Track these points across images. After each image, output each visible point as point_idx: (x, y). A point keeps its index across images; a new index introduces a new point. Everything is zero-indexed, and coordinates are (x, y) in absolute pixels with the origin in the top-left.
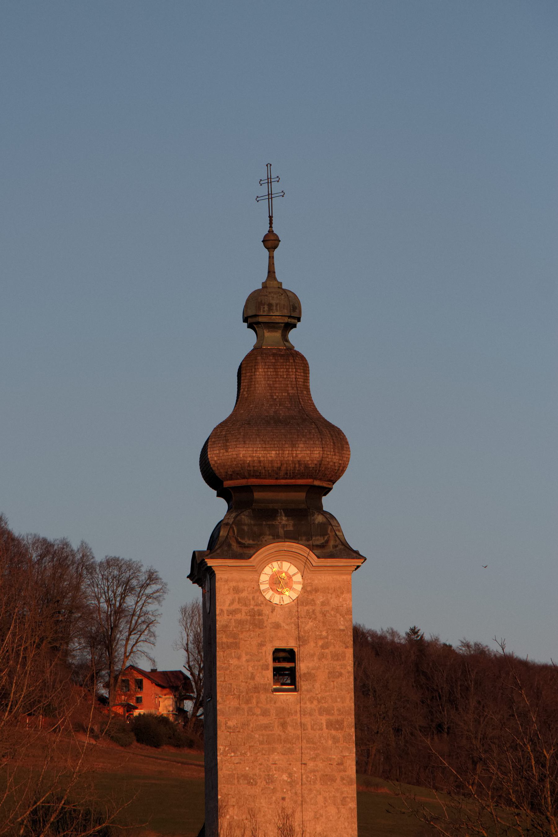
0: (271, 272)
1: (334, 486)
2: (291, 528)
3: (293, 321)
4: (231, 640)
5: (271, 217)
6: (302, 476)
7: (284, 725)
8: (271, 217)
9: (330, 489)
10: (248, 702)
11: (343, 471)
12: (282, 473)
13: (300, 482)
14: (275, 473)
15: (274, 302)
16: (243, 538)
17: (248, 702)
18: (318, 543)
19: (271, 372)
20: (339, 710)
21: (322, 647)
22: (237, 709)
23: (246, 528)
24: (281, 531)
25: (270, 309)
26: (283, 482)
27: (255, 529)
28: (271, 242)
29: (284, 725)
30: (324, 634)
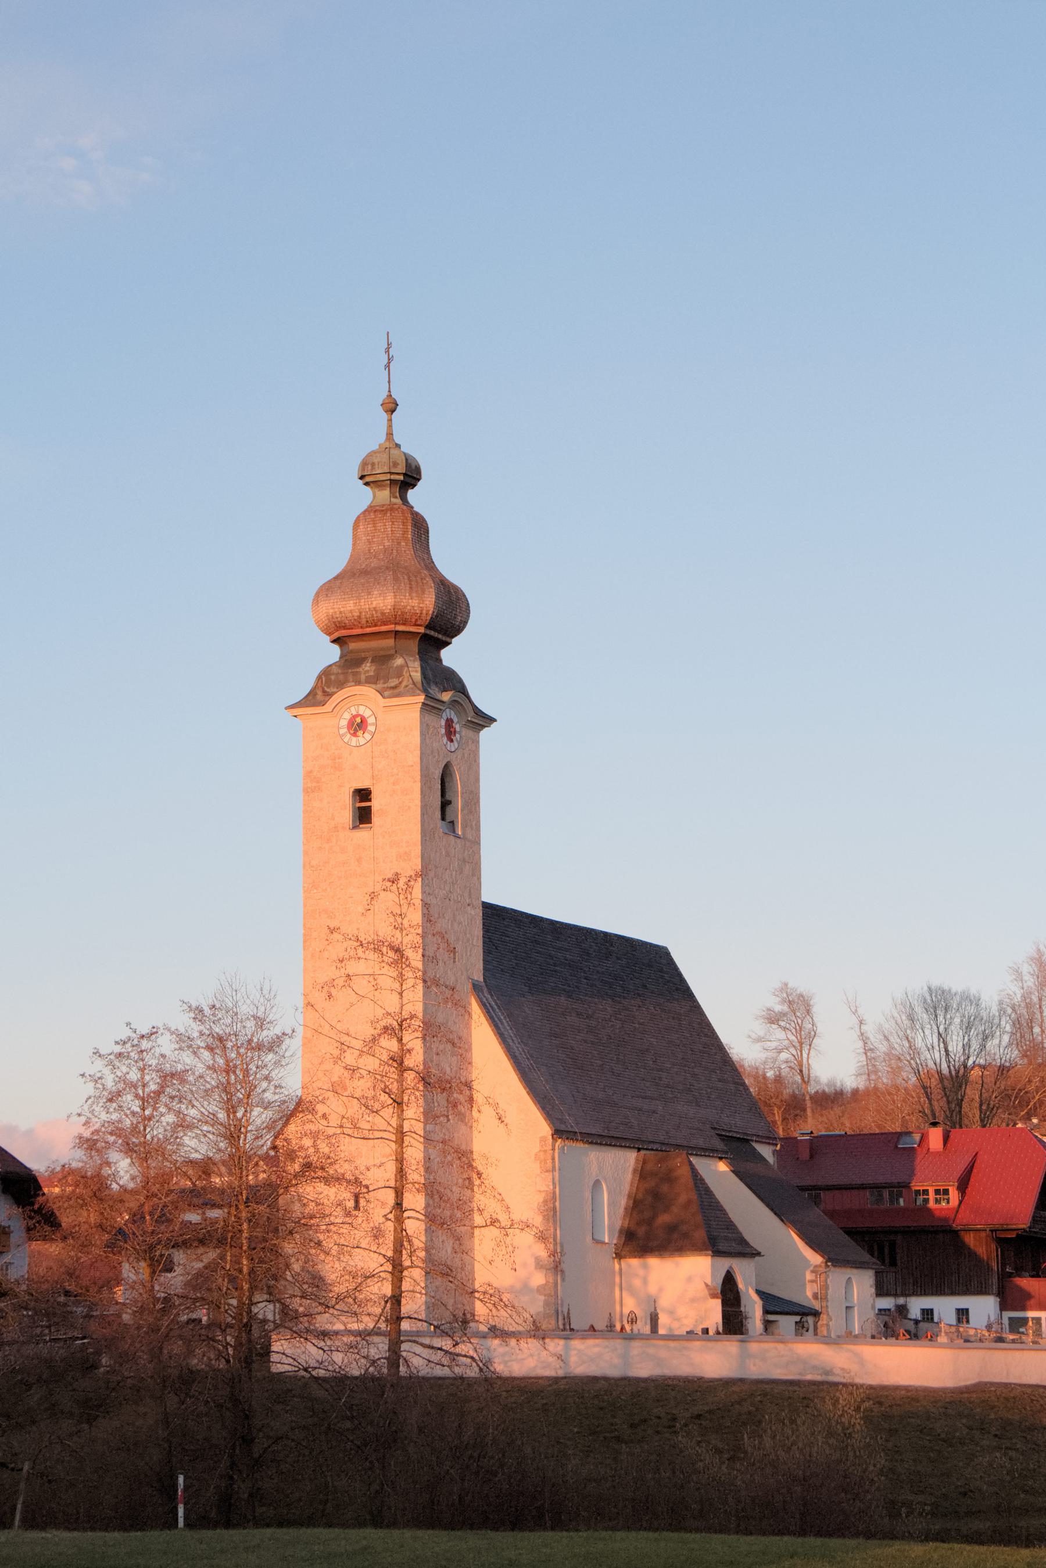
0: (390, 434)
1: (454, 640)
2: (372, 673)
3: (409, 480)
4: (314, 784)
5: (389, 382)
6: (385, 624)
7: (359, 860)
8: (389, 382)
9: (450, 643)
10: (329, 840)
11: (464, 627)
12: (364, 621)
13: (384, 628)
14: (357, 622)
15: (376, 461)
16: (328, 687)
17: (329, 840)
18: (393, 685)
19: (370, 528)
20: (407, 842)
21: (394, 784)
22: (320, 848)
23: (333, 677)
24: (363, 677)
25: (373, 468)
26: (368, 630)
27: (341, 677)
28: (391, 407)
29: (359, 860)
30: (395, 771)
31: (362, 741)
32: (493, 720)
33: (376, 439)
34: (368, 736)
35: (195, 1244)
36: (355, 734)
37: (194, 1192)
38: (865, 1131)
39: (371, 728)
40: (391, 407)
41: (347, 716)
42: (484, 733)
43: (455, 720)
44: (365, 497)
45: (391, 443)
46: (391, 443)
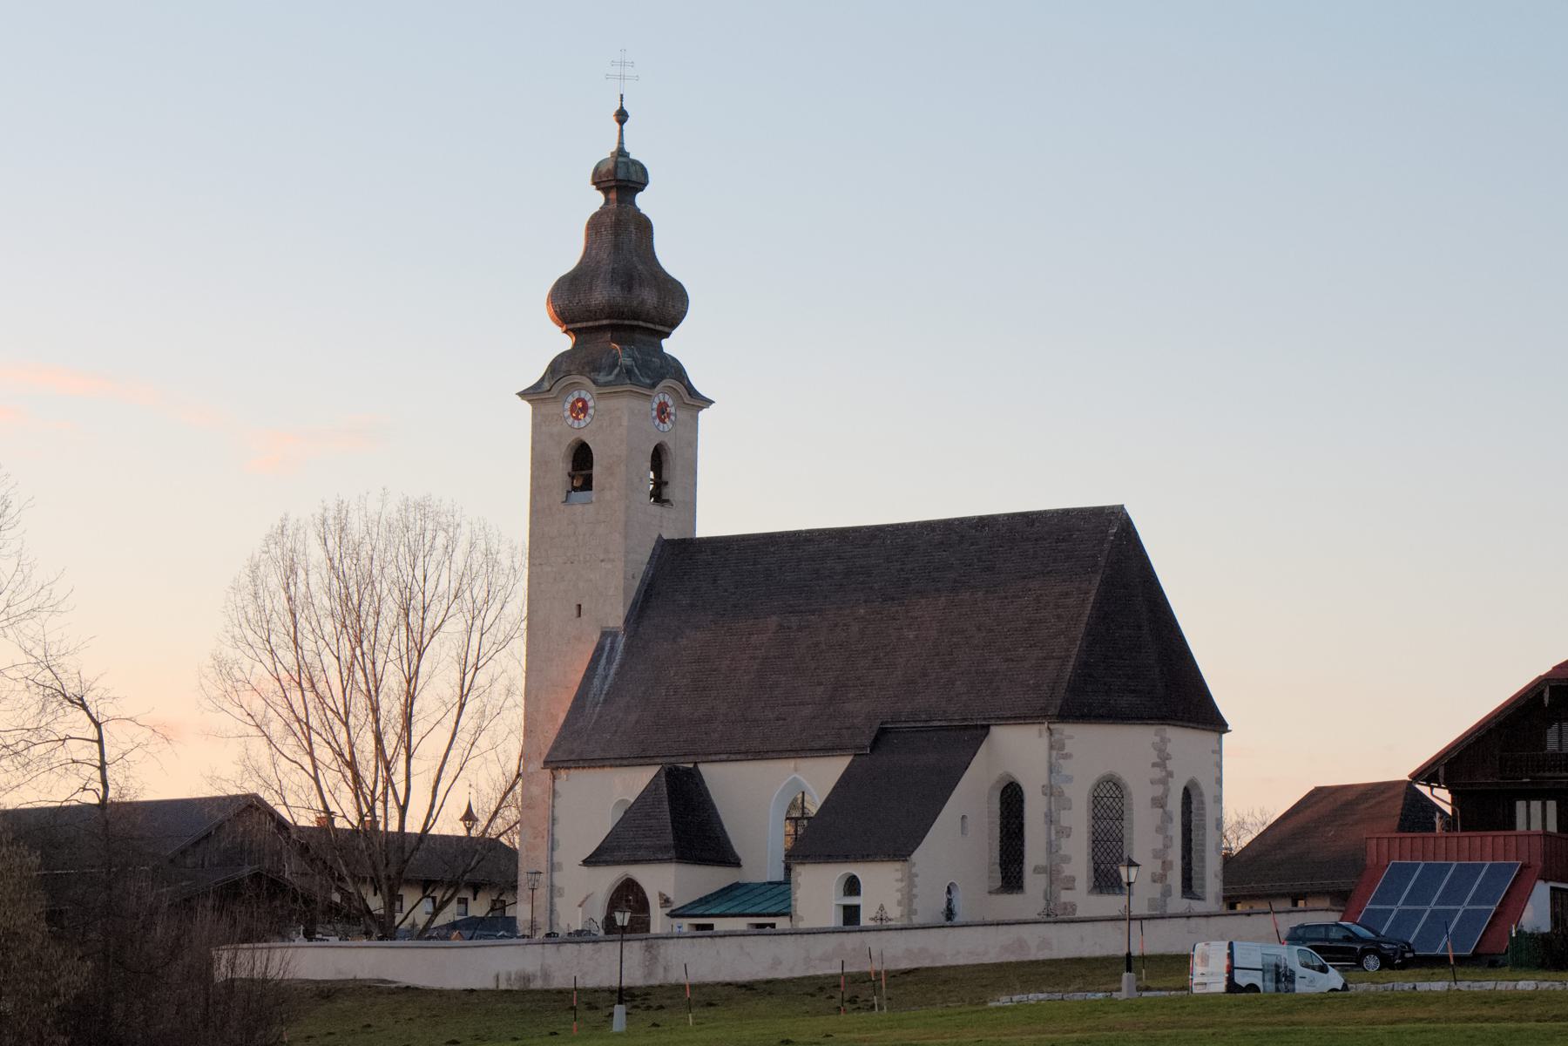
0: (621, 142)
28: (622, 116)
31: (583, 424)
32: (711, 402)
33: (606, 150)
34: (588, 419)
35: (1372, 962)
36: (577, 418)
37: (613, 311)
38: (537, 984)
39: (591, 411)
40: (622, 116)
41: (571, 399)
42: (703, 415)
43: (670, 403)
44: (597, 200)
45: (621, 152)
46: (621, 152)
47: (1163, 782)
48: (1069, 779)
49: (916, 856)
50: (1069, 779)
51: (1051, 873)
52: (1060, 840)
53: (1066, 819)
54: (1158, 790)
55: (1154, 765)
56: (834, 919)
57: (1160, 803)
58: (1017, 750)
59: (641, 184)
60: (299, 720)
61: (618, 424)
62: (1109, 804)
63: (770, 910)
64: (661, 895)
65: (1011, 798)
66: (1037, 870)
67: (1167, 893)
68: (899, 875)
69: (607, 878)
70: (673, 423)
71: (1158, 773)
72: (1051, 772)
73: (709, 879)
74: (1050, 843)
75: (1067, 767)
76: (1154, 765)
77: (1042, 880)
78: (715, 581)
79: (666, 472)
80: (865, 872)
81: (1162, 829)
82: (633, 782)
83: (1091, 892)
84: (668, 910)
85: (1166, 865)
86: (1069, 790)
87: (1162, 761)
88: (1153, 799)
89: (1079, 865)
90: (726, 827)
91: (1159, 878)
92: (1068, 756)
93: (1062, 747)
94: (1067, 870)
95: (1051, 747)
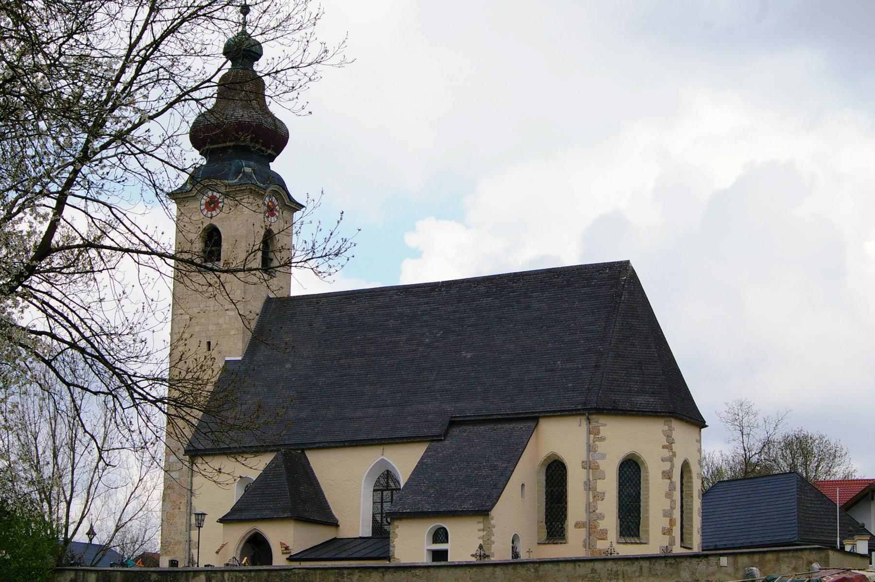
47: (670, 459)
48: (603, 456)
49: (495, 512)
50: (603, 456)
51: (591, 528)
52: (593, 501)
53: (600, 486)
54: (667, 466)
55: (664, 447)
56: (424, 559)
57: (667, 475)
58: (561, 437)
59: (258, 55)
60: (142, 152)
61: (240, 224)
62: (631, 470)
63: (372, 555)
64: (282, 544)
65: (555, 472)
66: (577, 525)
67: (672, 543)
68: (481, 526)
69: (240, 532)
70: (277, 217)
71: (666, 453)
72: (589, 451)
73: (317, 535)
74: (588, 505)
75: (601, 447)
76: (664, 447)
77: (582, 533)
78: (311, 325)
79: (271, 255)
80: (452, 526)
81: (669, 495)
82: (255, 467)
83: (628, 262)
84: (288, 556)
85: (672, 522)
86: (603, 464)
87: (669, 446)
88: (663, 472)
89: (610, 521)
90: (326, 496)
91: (668, 532)
92: (603, 439)
93: (599, 433)
94: (602, 525)
95: (590, 433)
